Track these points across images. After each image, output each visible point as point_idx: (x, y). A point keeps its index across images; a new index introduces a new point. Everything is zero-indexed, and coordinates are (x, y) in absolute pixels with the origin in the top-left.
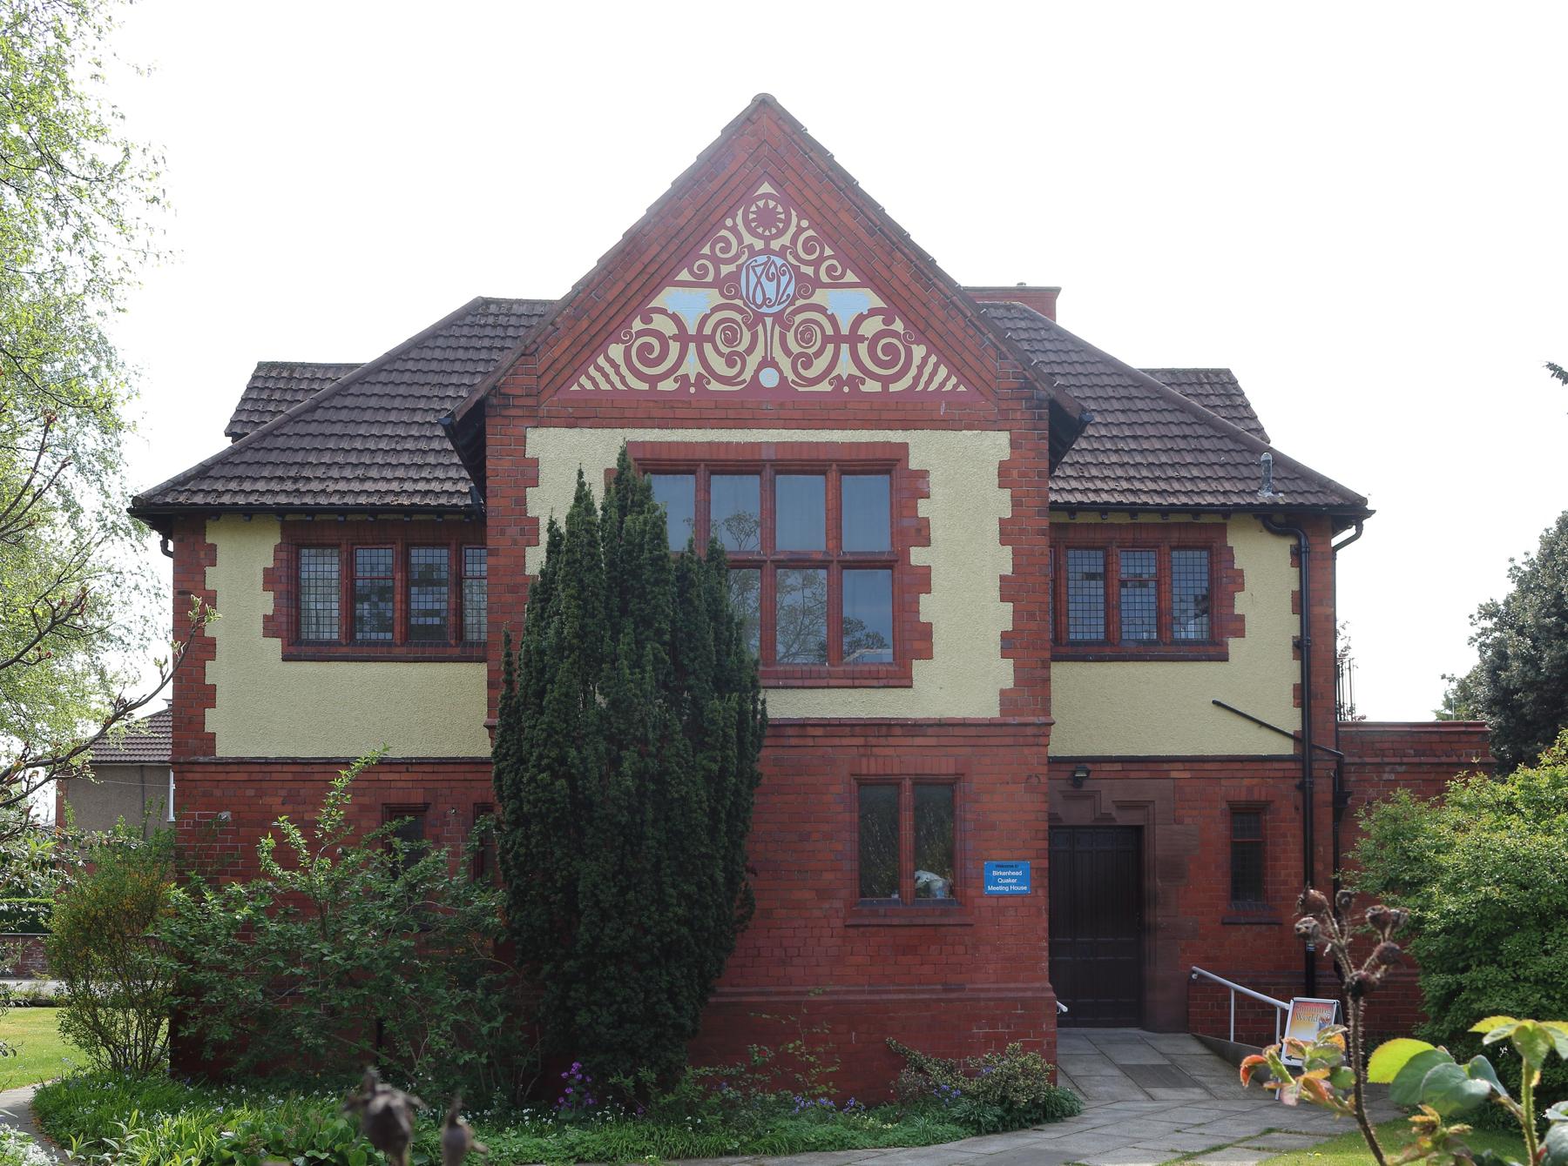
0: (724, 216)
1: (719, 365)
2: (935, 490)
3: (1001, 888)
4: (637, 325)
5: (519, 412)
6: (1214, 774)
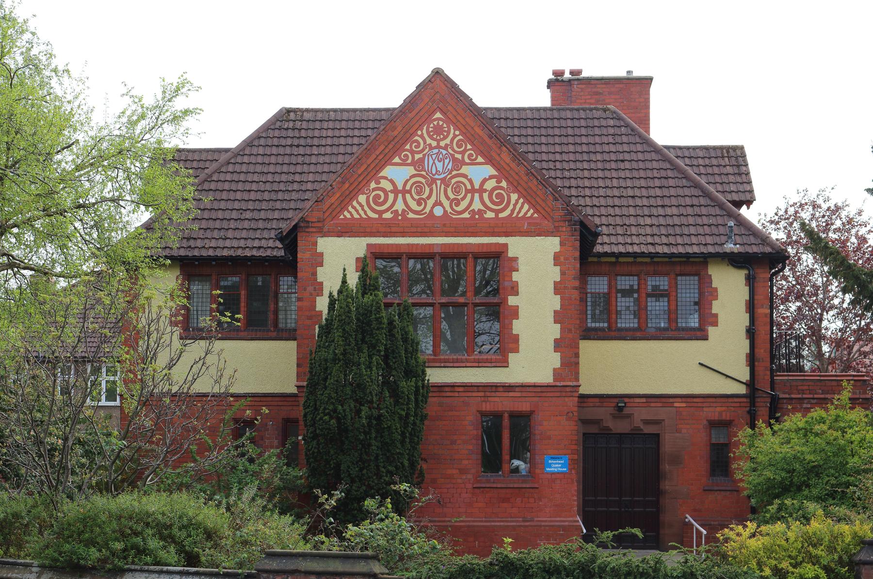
0: (417, 130)
1: (413, 205)
2: (521, 267)
3: (553, 469)
4: (373, 185)
5: (314, 230)
6: (699, 405)
